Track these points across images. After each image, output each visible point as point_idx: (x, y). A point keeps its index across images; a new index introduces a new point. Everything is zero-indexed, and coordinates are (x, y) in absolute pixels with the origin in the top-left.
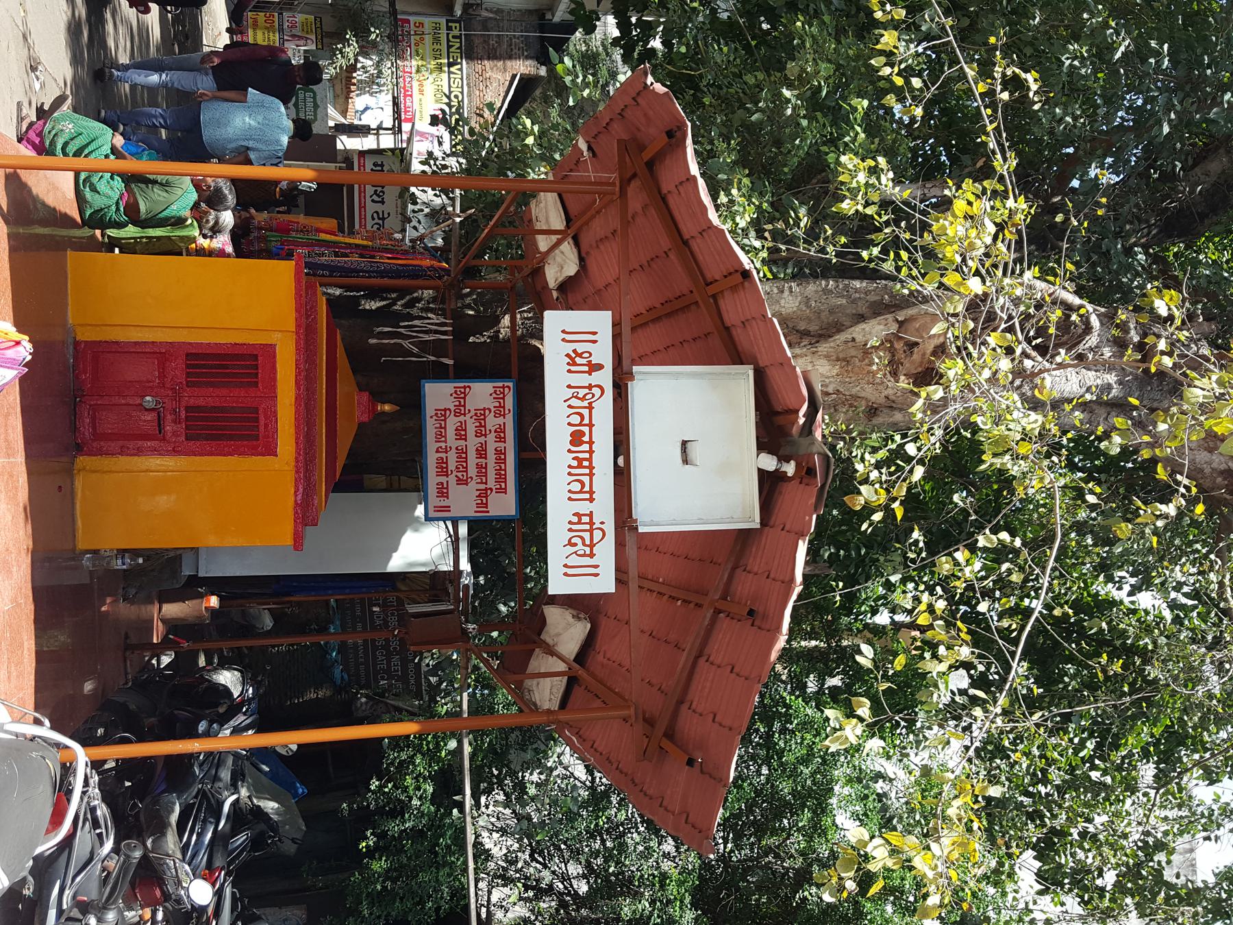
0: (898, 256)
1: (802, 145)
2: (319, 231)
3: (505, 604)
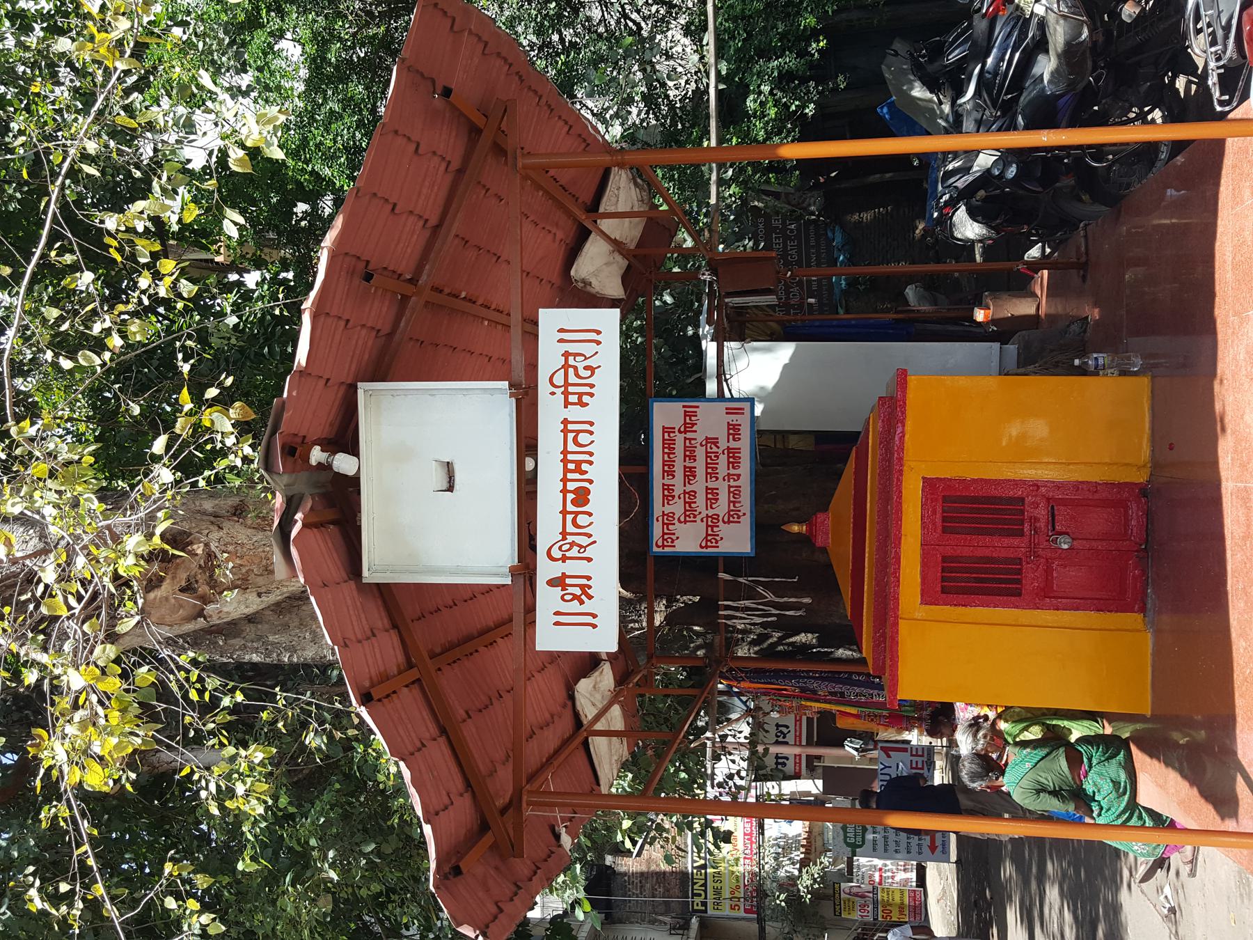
0: (201, 692)
1: (317, 816)
2: (857, 716)
3: (665, 303)
